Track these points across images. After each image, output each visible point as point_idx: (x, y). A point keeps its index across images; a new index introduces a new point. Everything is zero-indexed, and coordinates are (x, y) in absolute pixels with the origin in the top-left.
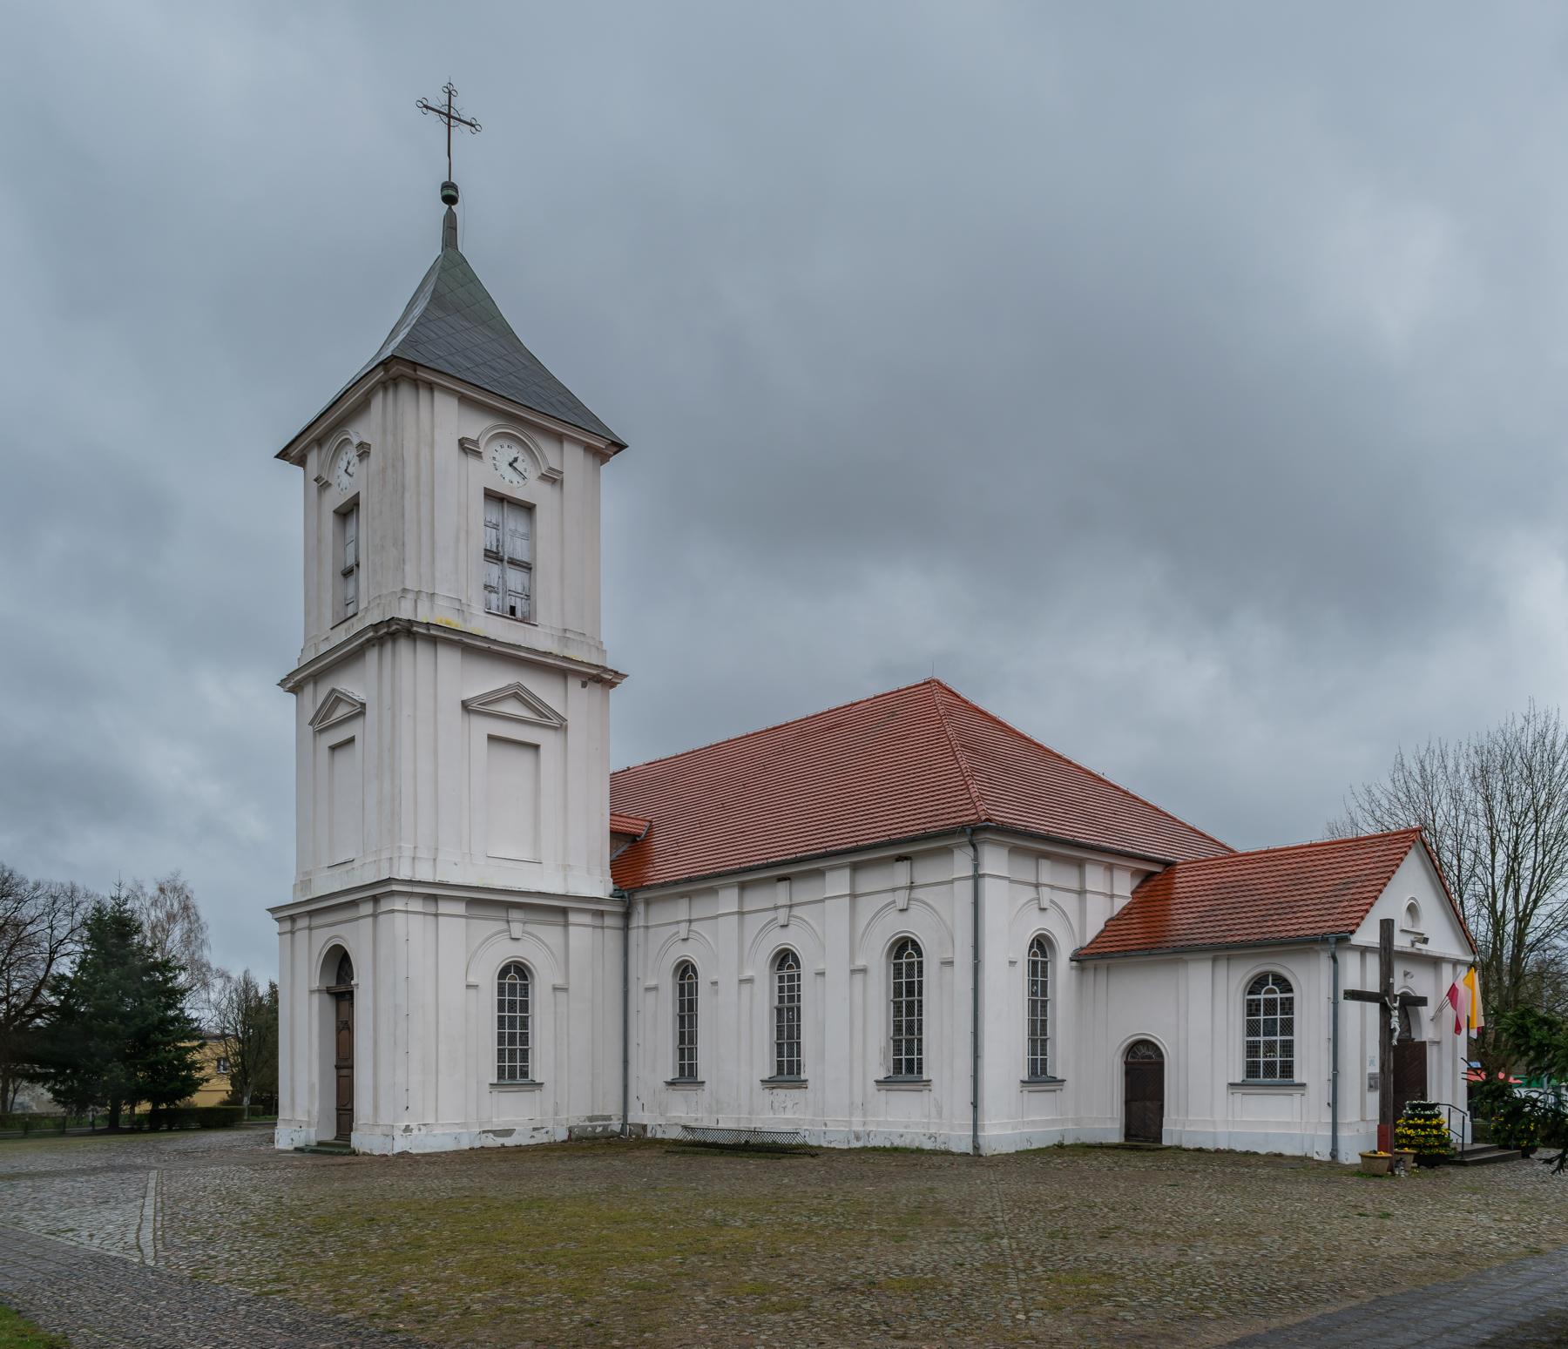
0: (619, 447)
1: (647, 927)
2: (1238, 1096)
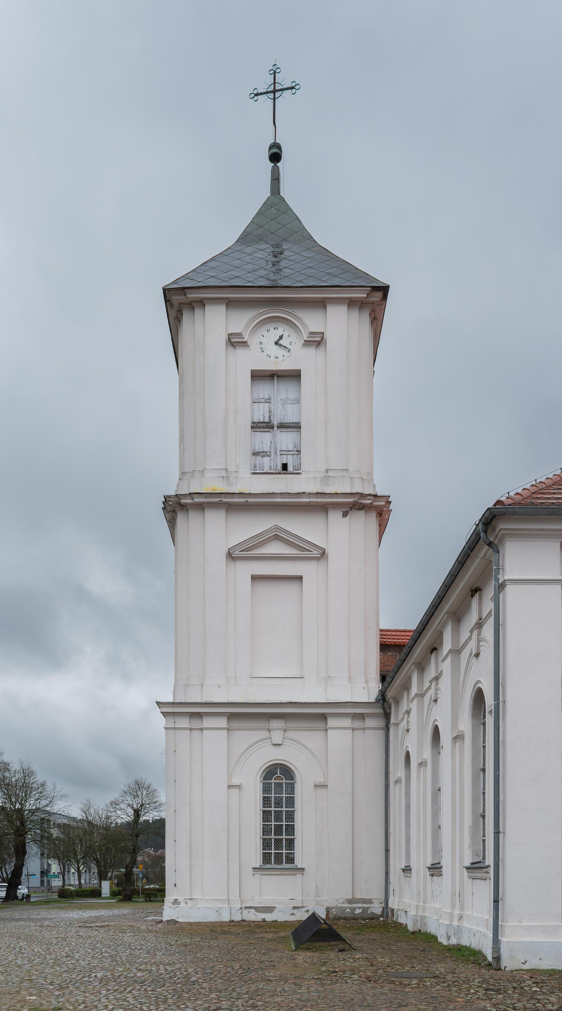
2: (258, 876)
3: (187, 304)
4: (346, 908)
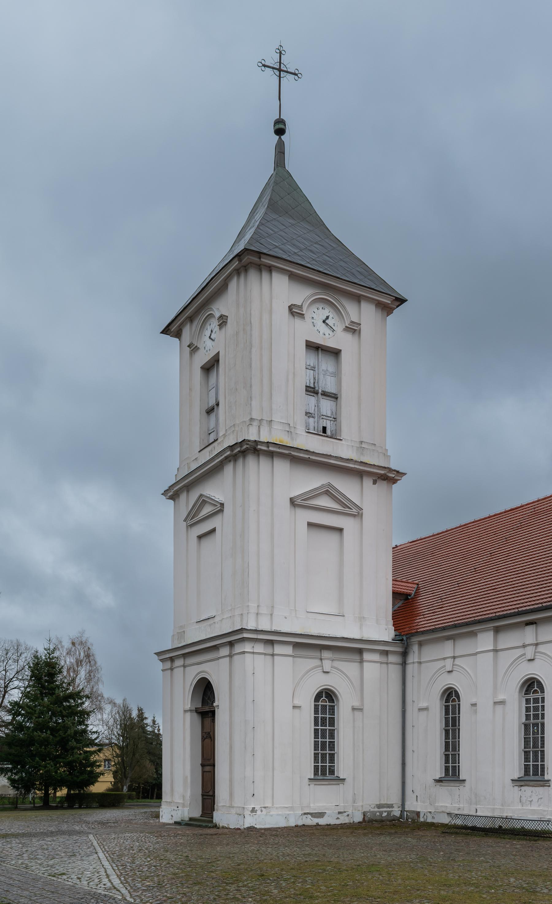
0: (401, 301)
1: (420, 663)
3: (256, 265)
4: (376, 812)
